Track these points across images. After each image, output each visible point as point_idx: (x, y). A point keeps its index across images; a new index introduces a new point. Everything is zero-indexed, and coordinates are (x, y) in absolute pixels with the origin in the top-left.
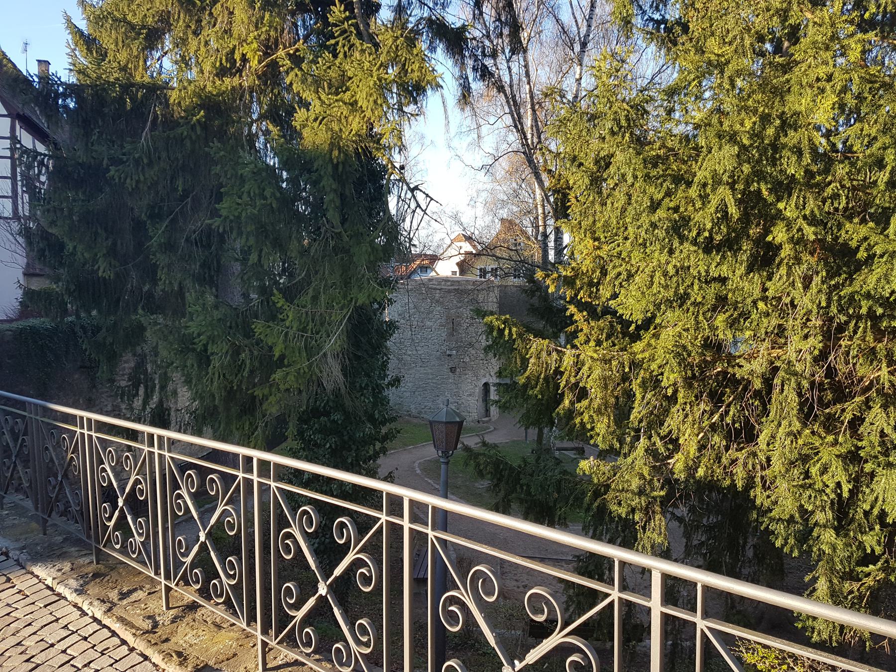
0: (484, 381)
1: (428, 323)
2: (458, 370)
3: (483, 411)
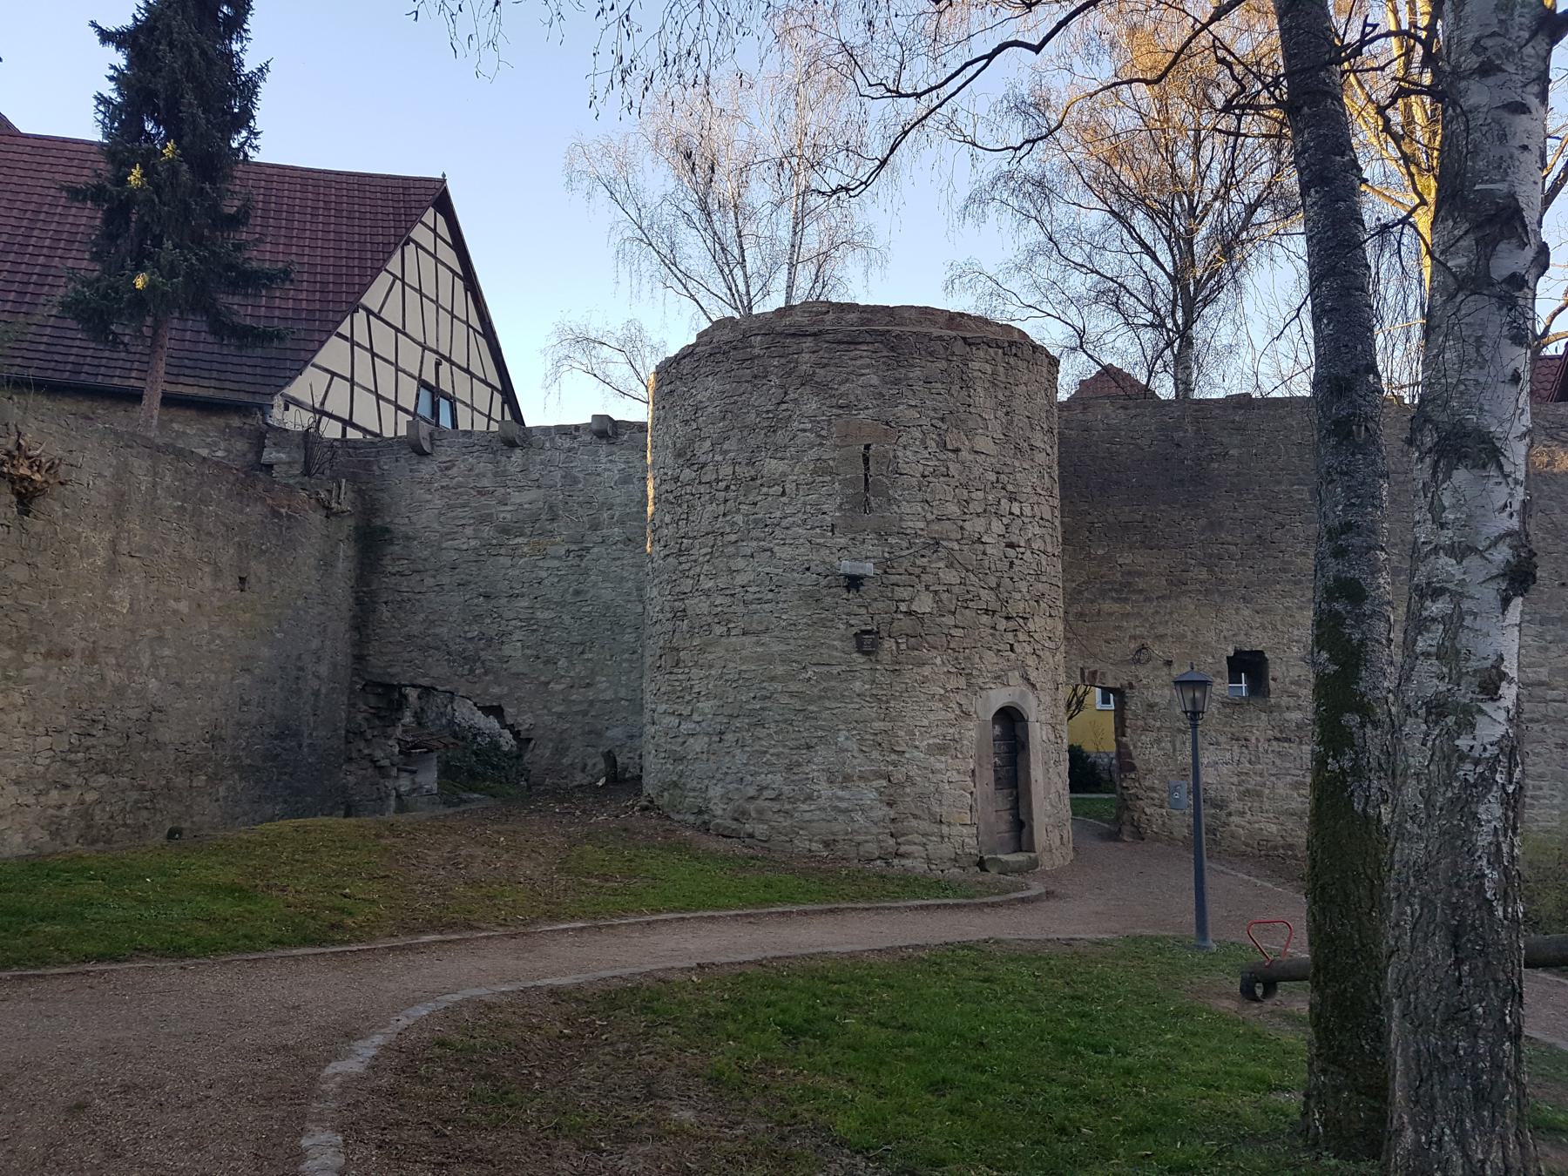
0: (999, 697)
1: (772, 466)
2: (889, 644)
3: (1003, 824)
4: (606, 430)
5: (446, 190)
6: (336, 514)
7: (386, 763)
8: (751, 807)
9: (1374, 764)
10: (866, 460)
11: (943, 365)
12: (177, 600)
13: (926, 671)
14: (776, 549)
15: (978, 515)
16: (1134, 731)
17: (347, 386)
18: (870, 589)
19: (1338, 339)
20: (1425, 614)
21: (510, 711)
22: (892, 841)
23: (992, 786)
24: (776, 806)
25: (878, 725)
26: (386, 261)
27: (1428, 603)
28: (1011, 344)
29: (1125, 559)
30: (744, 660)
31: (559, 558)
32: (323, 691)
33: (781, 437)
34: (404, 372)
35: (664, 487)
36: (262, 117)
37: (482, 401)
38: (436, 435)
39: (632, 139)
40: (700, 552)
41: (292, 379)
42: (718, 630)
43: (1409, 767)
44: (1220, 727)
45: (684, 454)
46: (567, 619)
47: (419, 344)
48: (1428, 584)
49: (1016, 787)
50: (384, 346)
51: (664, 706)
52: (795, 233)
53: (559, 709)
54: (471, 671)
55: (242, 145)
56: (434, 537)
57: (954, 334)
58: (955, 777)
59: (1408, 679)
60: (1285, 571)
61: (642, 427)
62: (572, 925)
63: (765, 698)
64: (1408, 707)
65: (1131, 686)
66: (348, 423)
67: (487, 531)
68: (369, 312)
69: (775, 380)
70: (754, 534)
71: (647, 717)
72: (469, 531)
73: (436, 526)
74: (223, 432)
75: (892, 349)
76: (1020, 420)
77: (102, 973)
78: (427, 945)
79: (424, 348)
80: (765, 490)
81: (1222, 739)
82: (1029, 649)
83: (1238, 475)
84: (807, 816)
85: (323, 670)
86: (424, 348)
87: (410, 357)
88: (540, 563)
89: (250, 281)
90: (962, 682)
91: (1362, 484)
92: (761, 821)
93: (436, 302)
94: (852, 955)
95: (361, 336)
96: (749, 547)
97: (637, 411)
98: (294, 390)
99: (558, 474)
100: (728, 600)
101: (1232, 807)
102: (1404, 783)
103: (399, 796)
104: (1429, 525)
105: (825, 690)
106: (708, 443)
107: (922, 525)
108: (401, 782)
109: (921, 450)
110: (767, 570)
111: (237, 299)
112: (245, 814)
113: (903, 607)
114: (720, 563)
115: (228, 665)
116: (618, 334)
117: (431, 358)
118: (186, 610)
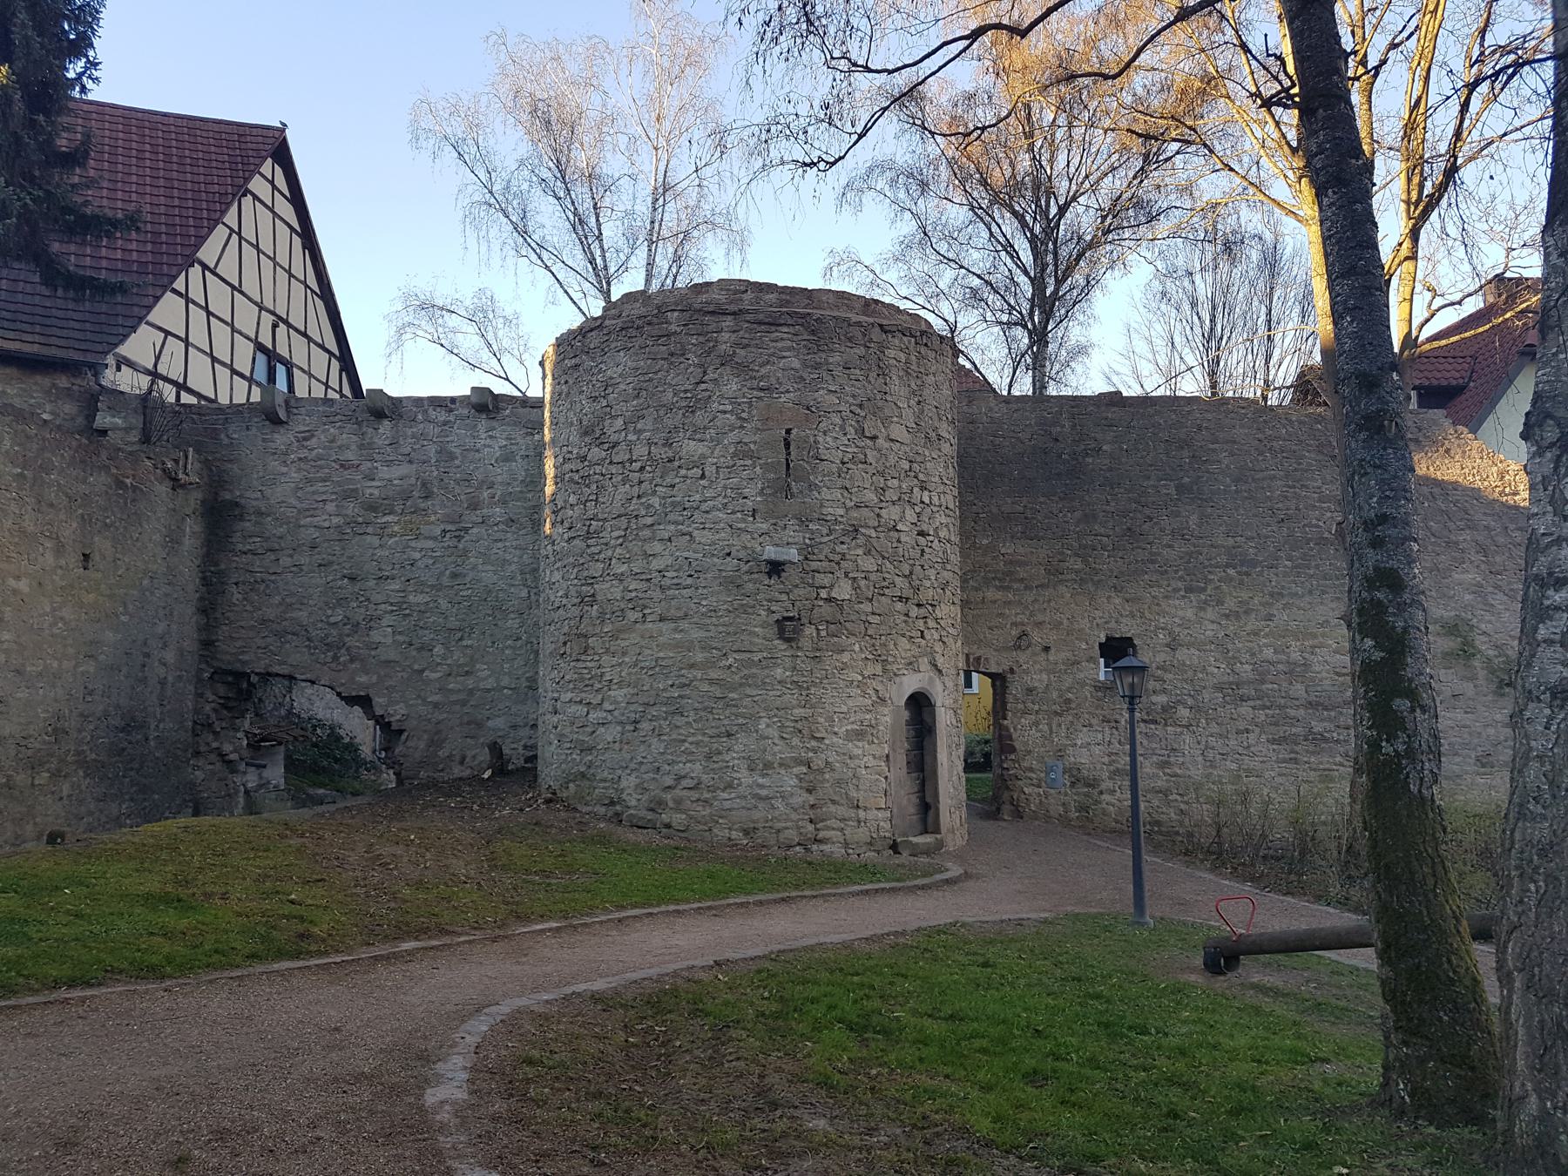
0: (911, 683)
1: (691, 448)
2: (809, 631)
3: (907, 801)
4: (485, 404)
5: (285, 139)
6: (183, 486)
7: (234, 757)
8: (668, 796)
9: (1424, 747)
10: (787, 445)
11: (861, 351)
12: (18, 578)
13: (846, 657)
14: (696, 533)
15: (894, 503)
16: (1014, 714)
17: (184, 346)
18: (791, 574)
19: (1362, 337)
20: (1547, 603)
21: (379, 702)
22: (811, 827)
23: (905, 770)
24: (695, 795)
25: (798, 712)
26: (223, 212)
27: (1550, 592)
28: (923, 333)
29: (1007, 548)
30: (661, 647)
31: (435, 539)
32: (170, 679)
33: (700, 418)
34: (241, 333)
35: (567, 467)
36: (102, 46)
37: (319, 369)
38: (293, 403)
39: (484, 99)
40: (611, 534)
41: (126, 336)
42: (633, 616)
43: (1531, 749)
44: (1092, 710)
45: (592, 432)
46: (444, 604)
47: (255, 303)
48: (1550, 574)
49: (922, 770)
50: (220, 304)
51: (569, 695)
52: (655, 210)
53: (436, 698)
54: (335, 658)
55: (80, 75)
56: (291, 513)
57: (871, 320)
58: (872, 762)
59: (1529, 665)
60: (1153, 562)
61: (538, 404)
62: (546, 925)
64: (1530, 692)
65: (1012, 671)
66: (182, 387)
67: (351, 508)
68: (205, 267)
69: (693, 359)
70: (671, 517)
71: (546, 706)
72: (331, 507)
73: (293, 501)
74: (48, 392)
75: (813, 332)
76: (930, 411)
77: (83, 1000)
78: (410, 953)
79: (261, 308)
80: (683, 472)
81: (1094, 721)
82: (936, 636)
83: (1110, 469)
84: (727, 805)
85: (170, 656)
86: (261, 308)
87: (246, 317)
88: (413, 544)
89: (88, 226)
90: (878, 669)
91: (1395, 477)
92: (678, 810)
93: (273, 259)
94: (846, 945)
95: (196, 293)
96: (666, 531)
97: (536, 386)
98: (126, 349)
99: (432, 450)
100: (645, 585)
101: (1103, 786)
102: (1526, 765)
103: (247, 792)
104: (1549, 517)
105: (746, 677)
106: (620, 422)
107: (841, 511)
108: (249, 777)
109: (840, 436)
110: (686, 554)
111: (73, 248)
112: (91, 813)
113: (824, 594)
114: (635, 547)
115: (71, 651)
116: (468, 303)
117: (268, 319)
118: (26, 590)
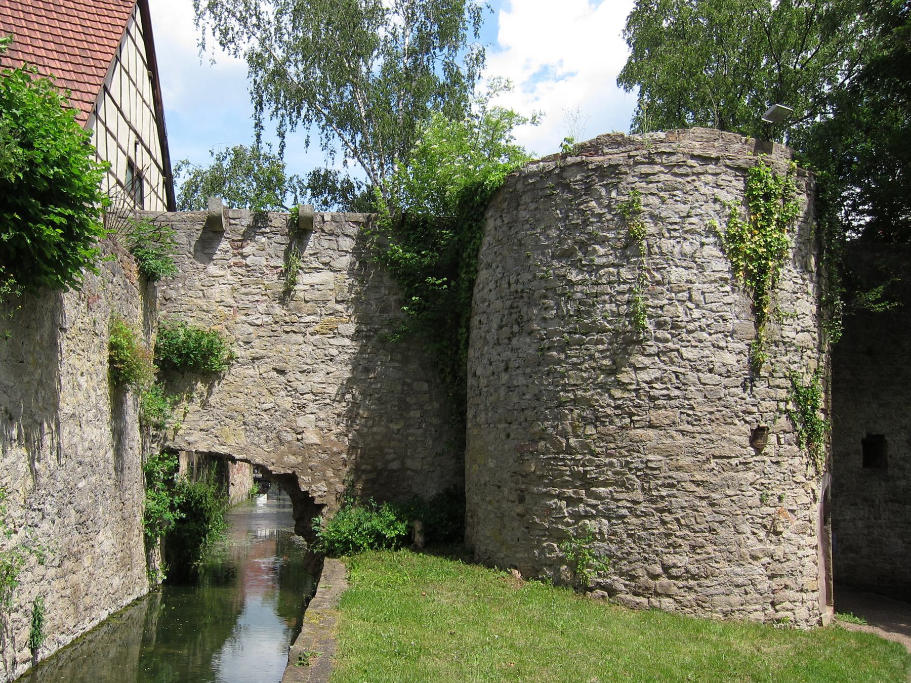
2: (773, 439)
63: (672, 486)
72: (262, 307)
